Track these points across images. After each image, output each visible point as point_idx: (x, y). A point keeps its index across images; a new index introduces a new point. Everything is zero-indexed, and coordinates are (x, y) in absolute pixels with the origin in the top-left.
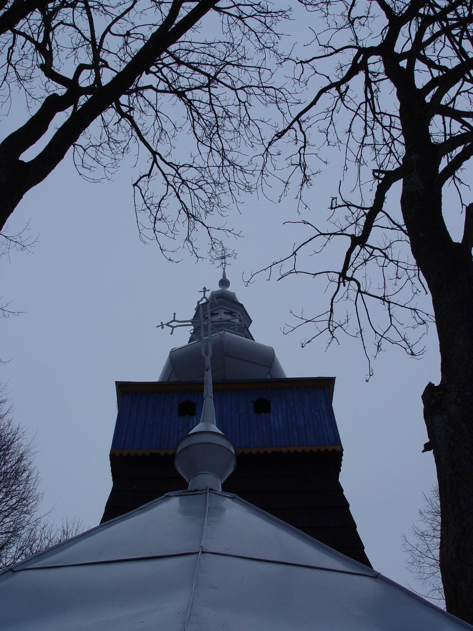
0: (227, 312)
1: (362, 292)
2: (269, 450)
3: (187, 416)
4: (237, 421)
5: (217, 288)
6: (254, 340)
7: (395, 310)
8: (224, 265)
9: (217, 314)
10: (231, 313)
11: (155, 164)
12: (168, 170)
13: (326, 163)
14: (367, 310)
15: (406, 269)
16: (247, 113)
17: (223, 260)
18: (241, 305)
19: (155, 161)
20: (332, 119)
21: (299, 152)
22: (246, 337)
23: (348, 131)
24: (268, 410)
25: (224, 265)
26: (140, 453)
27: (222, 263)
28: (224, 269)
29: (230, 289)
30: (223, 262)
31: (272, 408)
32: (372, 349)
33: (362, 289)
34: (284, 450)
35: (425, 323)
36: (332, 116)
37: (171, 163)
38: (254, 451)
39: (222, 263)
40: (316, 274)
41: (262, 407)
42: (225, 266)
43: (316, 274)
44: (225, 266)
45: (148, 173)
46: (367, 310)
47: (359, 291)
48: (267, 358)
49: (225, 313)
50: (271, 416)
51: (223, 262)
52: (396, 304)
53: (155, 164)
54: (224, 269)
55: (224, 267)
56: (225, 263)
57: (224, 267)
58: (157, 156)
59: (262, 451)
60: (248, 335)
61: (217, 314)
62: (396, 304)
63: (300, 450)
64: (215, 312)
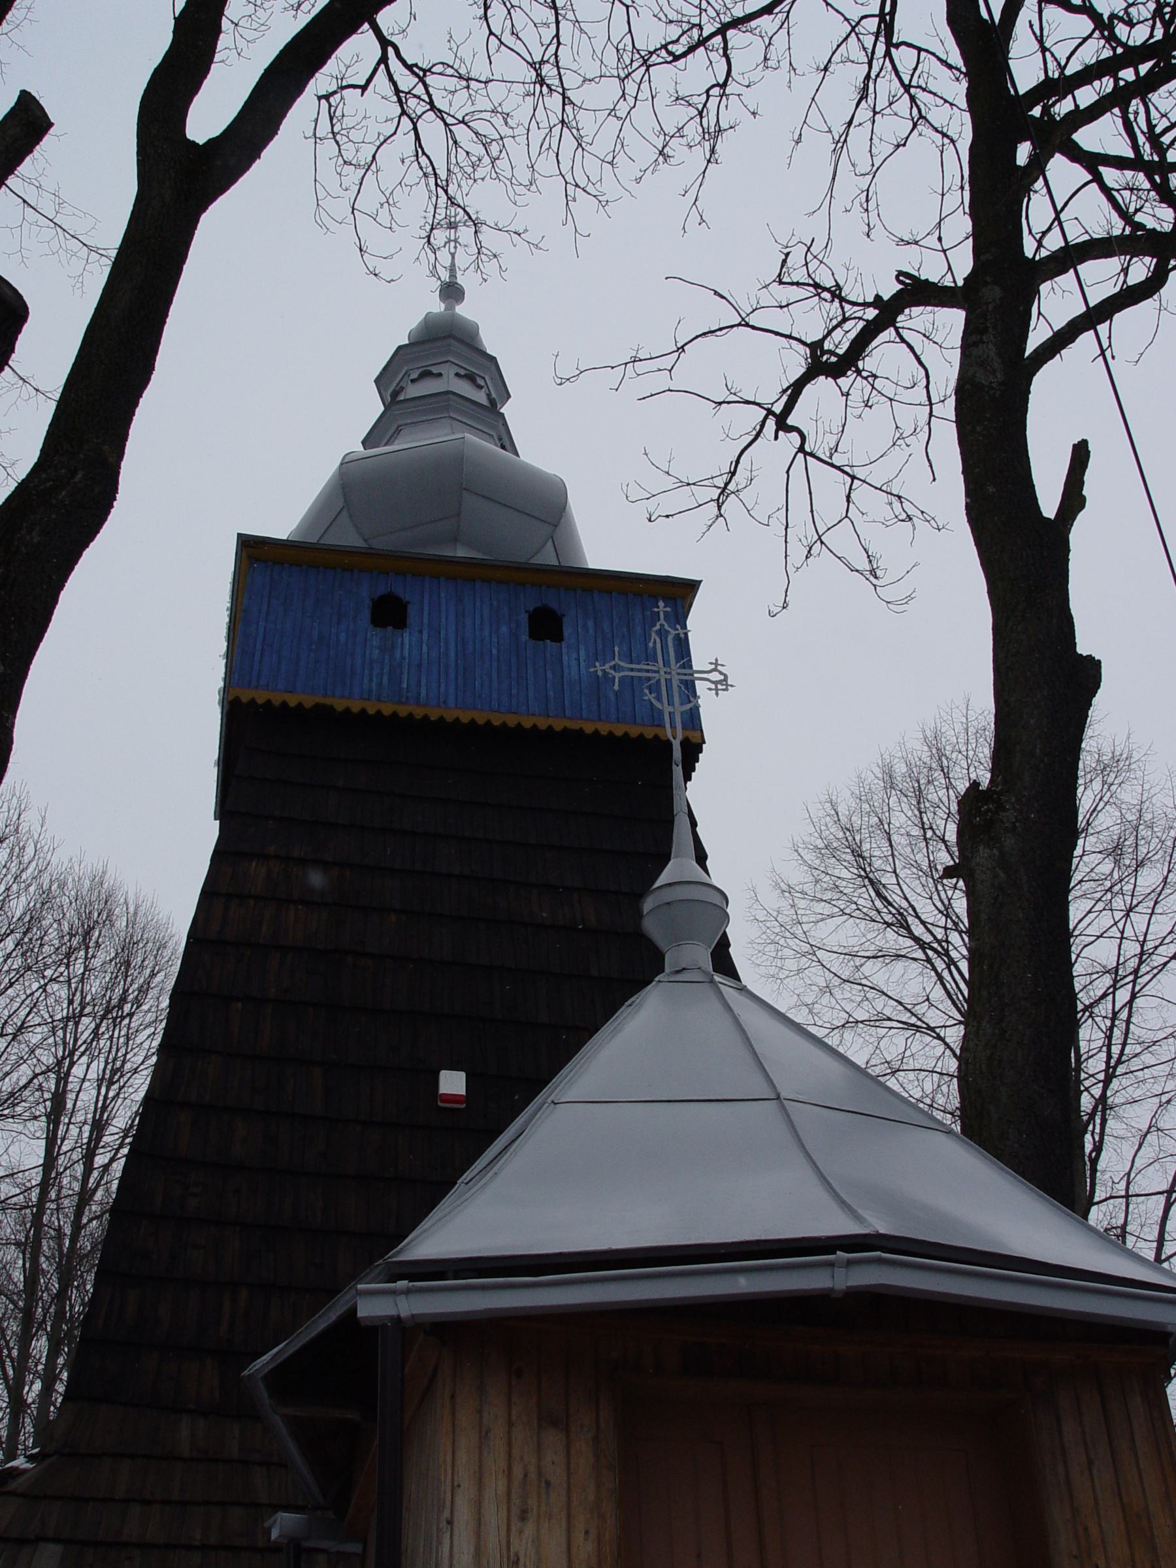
0: (463, 372)
1: (806, 454)
2: (559, 725)
3: (390, 628)
4: (494, 651)
5: (437, 306)
6: (517, 454)
7: (861, 493)
8: (452, 244)
9: (440, 375)
10: (471, 378)
11: (382, 66)
12: (406, 81)
13: (754, 113)
14: (810, 493)
15: (891, 400)
16: (630, 31)
17: (453, 231)
18: (493, 360)
19: (384, 59)
20: (787, 17)
21: (707, 92)
22: (503, 447)
23: (822, 67)
24: (557, 636)
25: (452, 244)
26: (293, 701)
27: (450, 241)
28: (453, 255)
29: (461, 310)
30: (452, 238)
31: (567, 631)
32: (797, 552)
33: (807, 449)
34: (589, 728)
35: (910, 519)
36: (788, 12)
37: (416, 65)
38: (527, 723)
39: (450, 241)
40: (720, 403)
41: (546, 625)
42: (455, 247)
43: (720, 403)
44: (455, 247)
45: (363, 83)
46: (810, 493)
47: (801, 449)
48: (547, 506)
49: (457, 375)
50: (564, 650)
51: (452, 238)
52: (864, 481)
53: (382, 66)
54: (453, 255)
55: (452, 250)
56: (456, 241)
57: (452, 250)
58: (390, 50)
59: (543, 724)
60: (507, 445)
61: (440, 375)
62: (864, 481)
63: (619, 731)
64: (435, 370)
